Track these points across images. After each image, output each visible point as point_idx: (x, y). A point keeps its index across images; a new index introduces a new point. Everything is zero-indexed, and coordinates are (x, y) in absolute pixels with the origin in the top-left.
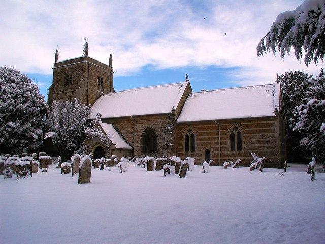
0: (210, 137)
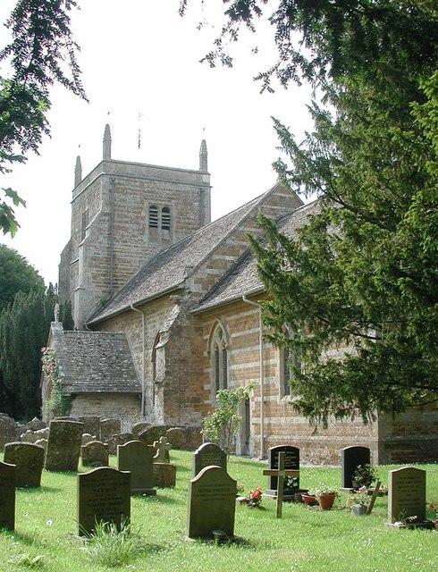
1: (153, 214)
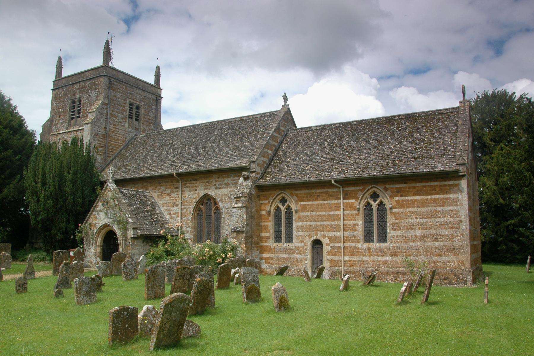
0: (323, 213)
1: (131, 109)
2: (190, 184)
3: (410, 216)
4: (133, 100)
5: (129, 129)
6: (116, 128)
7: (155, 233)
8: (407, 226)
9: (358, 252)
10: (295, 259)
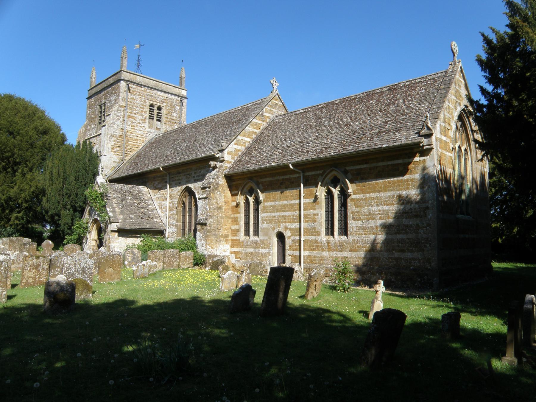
0: (285, 202)
1: (151, 110)
2: (175, 177)
3: (371, 203)
4: (154, 101)
5: (149, 129)
6: (134, 129)
7: (137, 227)
8: (367, 215)
9: (317, 246)
10: (260, 253)
